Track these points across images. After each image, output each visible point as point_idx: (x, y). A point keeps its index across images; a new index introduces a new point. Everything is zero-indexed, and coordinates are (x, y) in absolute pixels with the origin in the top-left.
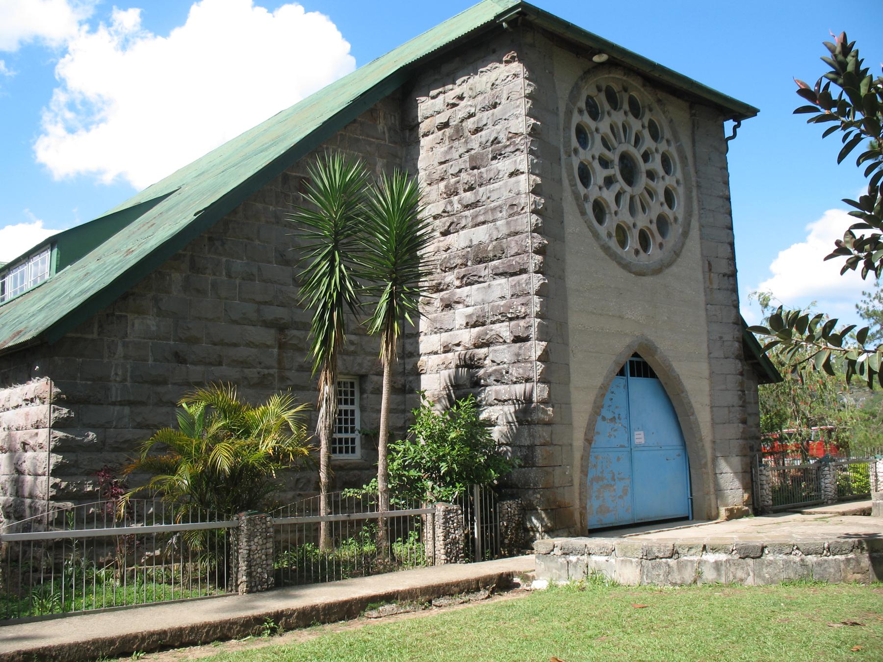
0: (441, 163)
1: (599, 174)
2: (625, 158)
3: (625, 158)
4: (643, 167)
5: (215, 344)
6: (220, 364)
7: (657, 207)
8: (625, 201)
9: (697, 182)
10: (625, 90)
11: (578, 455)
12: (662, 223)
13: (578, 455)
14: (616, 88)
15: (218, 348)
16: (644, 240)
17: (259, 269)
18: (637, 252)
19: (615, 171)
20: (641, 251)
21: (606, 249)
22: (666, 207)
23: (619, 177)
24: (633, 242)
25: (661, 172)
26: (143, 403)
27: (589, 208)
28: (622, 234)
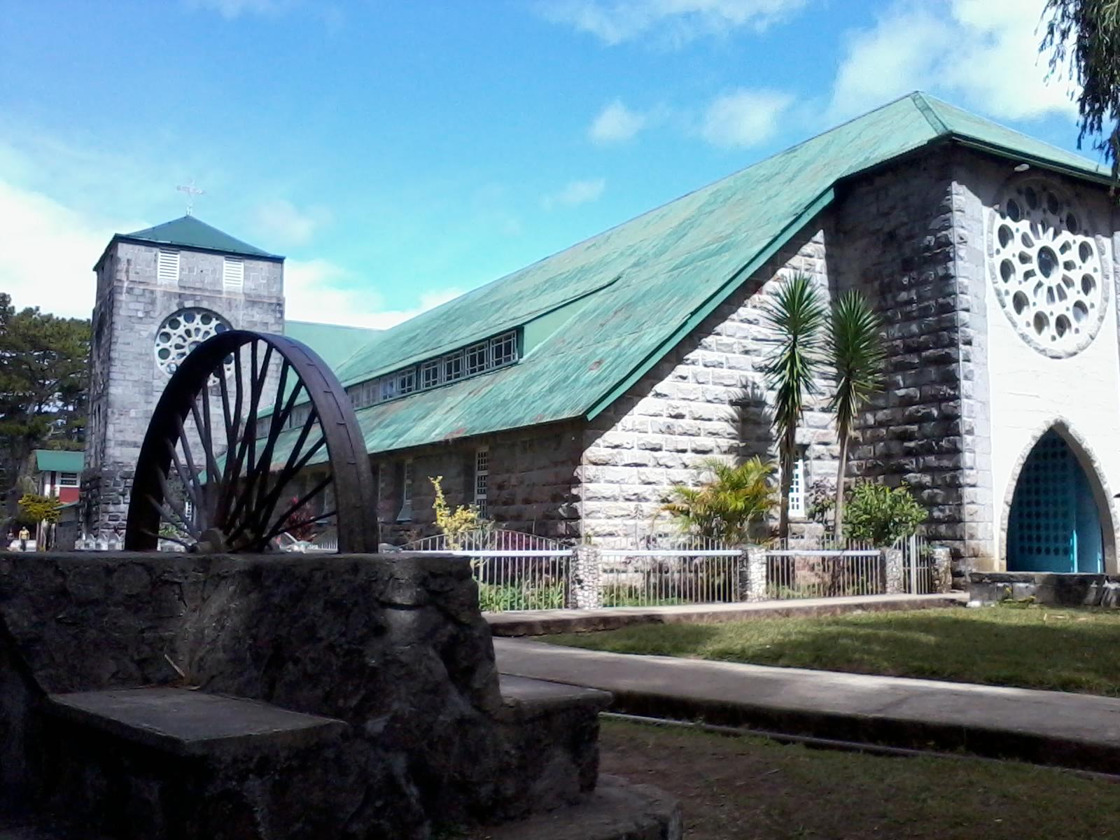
0: (874, 265)
1: (1020, 269)
2: (1045, 251)
3: (1045, 251)
4: (1062, 259)
5: (695, 419)
6: (699, 435)
7: (1074, 294)
8: (1043, 291)
9: (1115, 269)
10: (1045, 189)
11: (870, 631)
12: (1062, 324)
13: (870, 631)
14: (1036, 189)
15: (698, 422)
16: (1062, 324)
17: (727, 359)
18: (1054, 338)
19: (1034, 265)
20: (1057, 337)
21: (1024, 337)
22: (1032, 328)
23: (1037, 271)
24: (1051, 329)
25: (1078, 261)
26: (645, 465)
27: (1009, 300)
28: (1040, 321)
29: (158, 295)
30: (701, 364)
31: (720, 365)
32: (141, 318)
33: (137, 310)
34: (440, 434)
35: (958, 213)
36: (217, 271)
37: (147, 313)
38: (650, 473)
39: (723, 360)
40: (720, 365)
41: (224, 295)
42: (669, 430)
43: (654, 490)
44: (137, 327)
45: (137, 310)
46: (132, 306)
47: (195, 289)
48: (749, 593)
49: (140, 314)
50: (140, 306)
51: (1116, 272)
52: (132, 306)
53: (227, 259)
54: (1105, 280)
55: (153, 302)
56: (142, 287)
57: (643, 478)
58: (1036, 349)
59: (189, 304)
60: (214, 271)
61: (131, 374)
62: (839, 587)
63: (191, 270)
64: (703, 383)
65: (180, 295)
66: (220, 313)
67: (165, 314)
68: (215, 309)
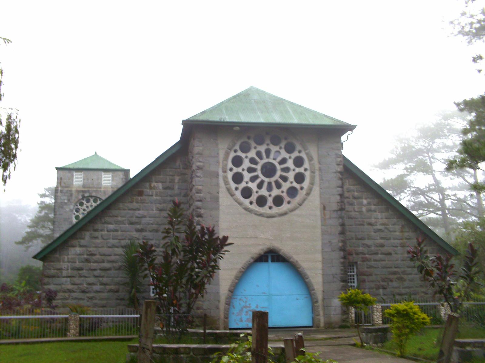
12: (262, 201)
29: (74, 192)
30: (106, 230)
31: (116, 231)
32: (66, 203)
33: (64, 199)
34: (423, 219)
35: (198, 156)
36: (100, 179)
37: (69, 200)
38: (76, 280)
39: (118, 228)
40: (116, 231)
41: (102, 190)
42: (87, 261)
43: (79, 288)
44: (65, 207)
45: (64, 199)
46: (62, 198)
47: (89, 187)
48: (68, 333)
49: (66, 201)
50: (66, 198)
51: (320, 169)
52: (62, 198)
53: (104, 172)
54: (312, 174)
55: (71, 195)
56: (66, 189)
57: (72, 282)
58: (256, 214)
59: (87, 195)
60: (98, 179)
61: (62, 228)
62: (125, 328)
63: (88, 179)
64: (106, 239)
65: (83, 191)
66: (101, 197)
67: (76, 200)
68: (99, 196)
